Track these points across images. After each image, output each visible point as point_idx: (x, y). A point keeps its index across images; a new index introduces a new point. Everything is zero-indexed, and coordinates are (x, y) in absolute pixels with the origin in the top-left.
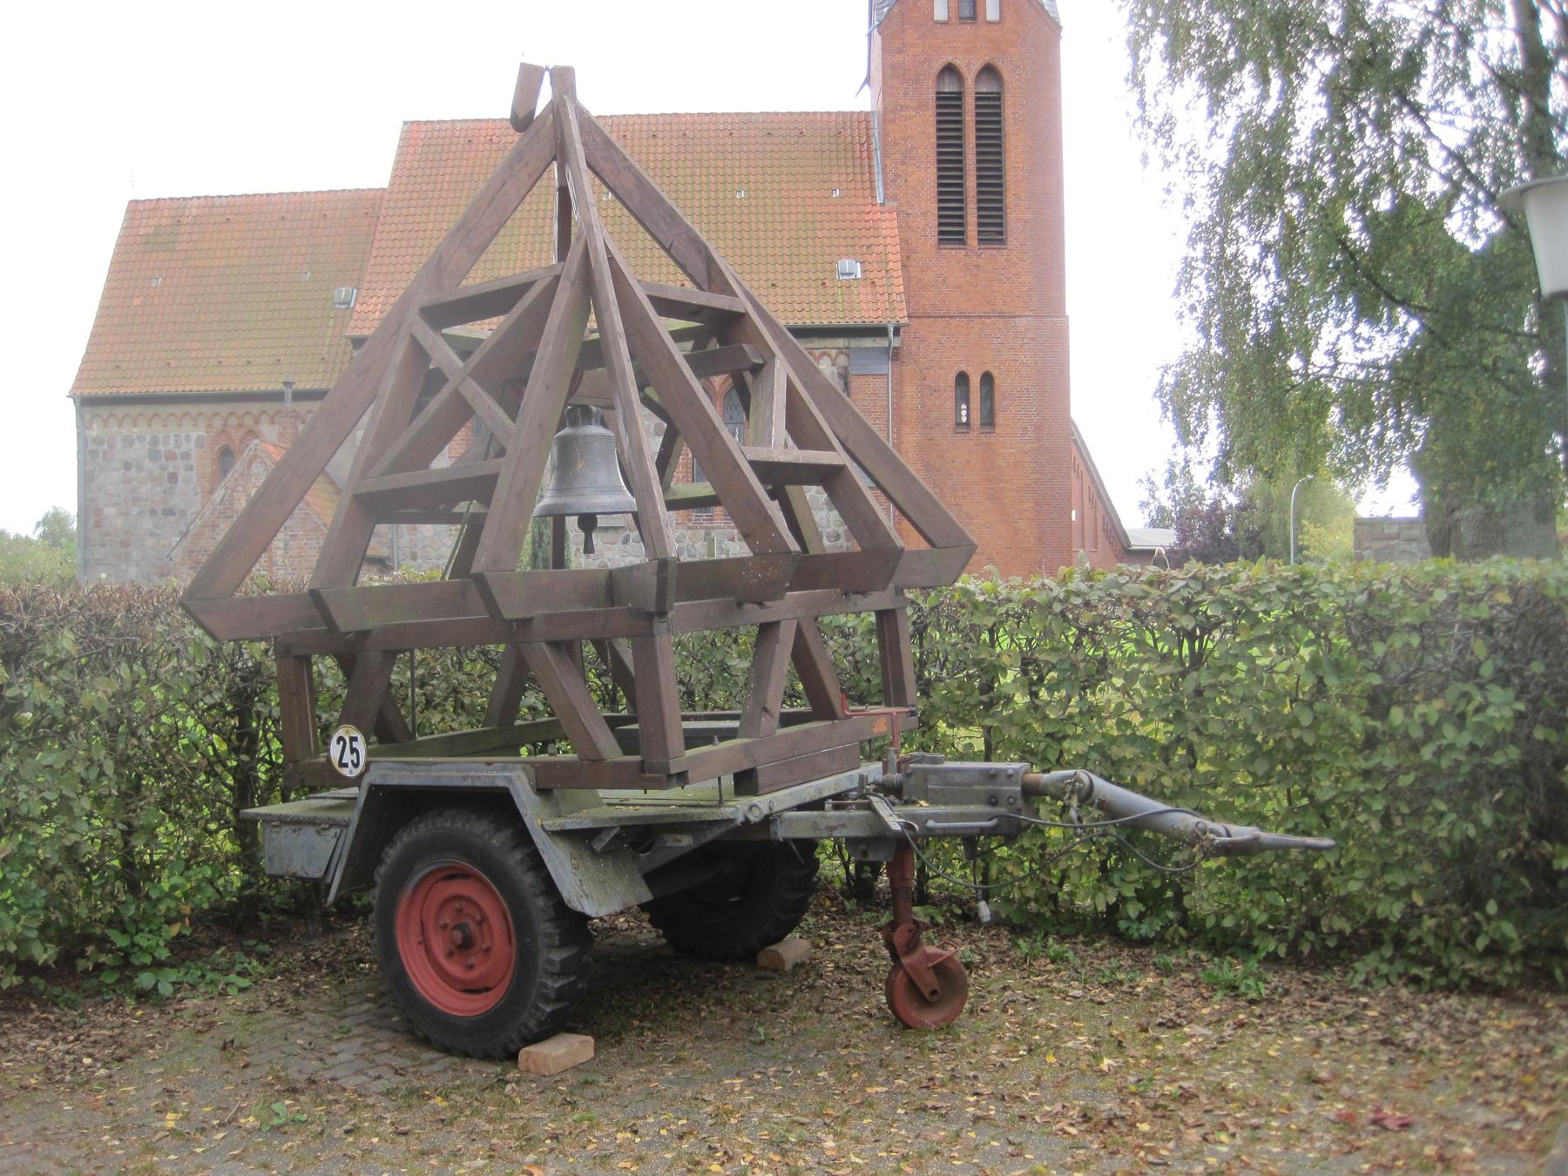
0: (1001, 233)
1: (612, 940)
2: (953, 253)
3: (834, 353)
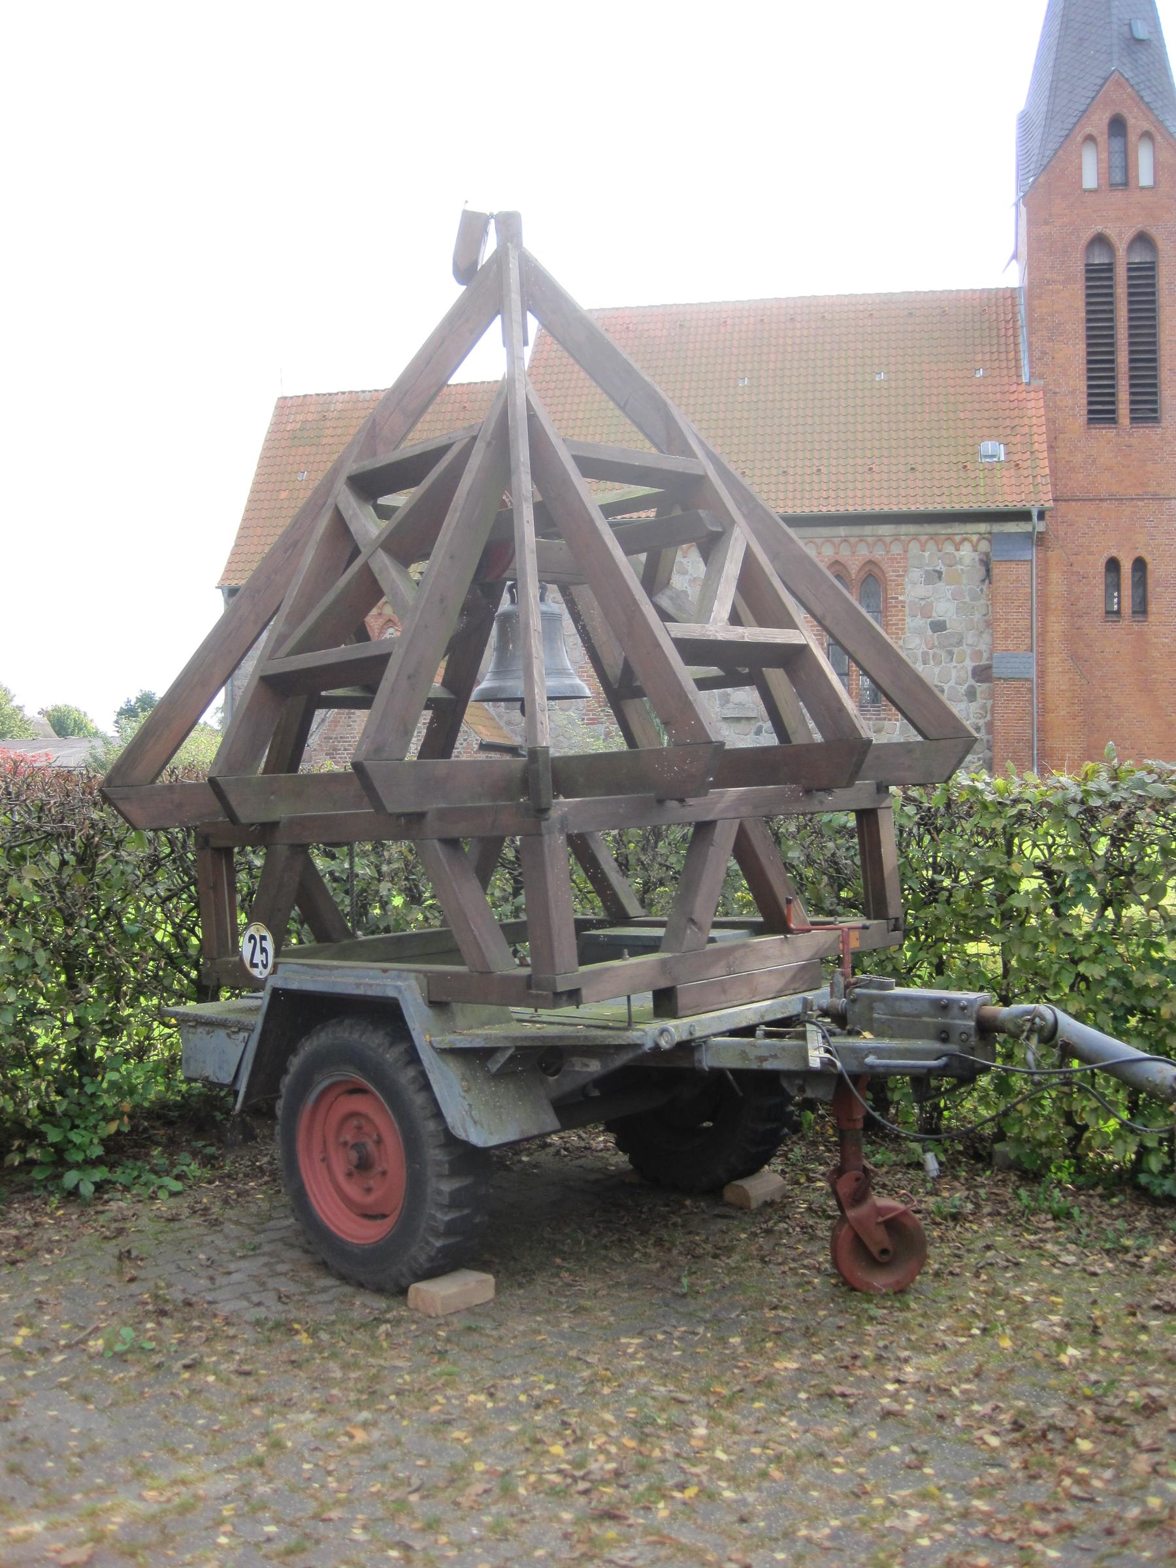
0: (1155, 411)
1: (581, 1161)
2: (1105, 433)
3: (975, 538)
